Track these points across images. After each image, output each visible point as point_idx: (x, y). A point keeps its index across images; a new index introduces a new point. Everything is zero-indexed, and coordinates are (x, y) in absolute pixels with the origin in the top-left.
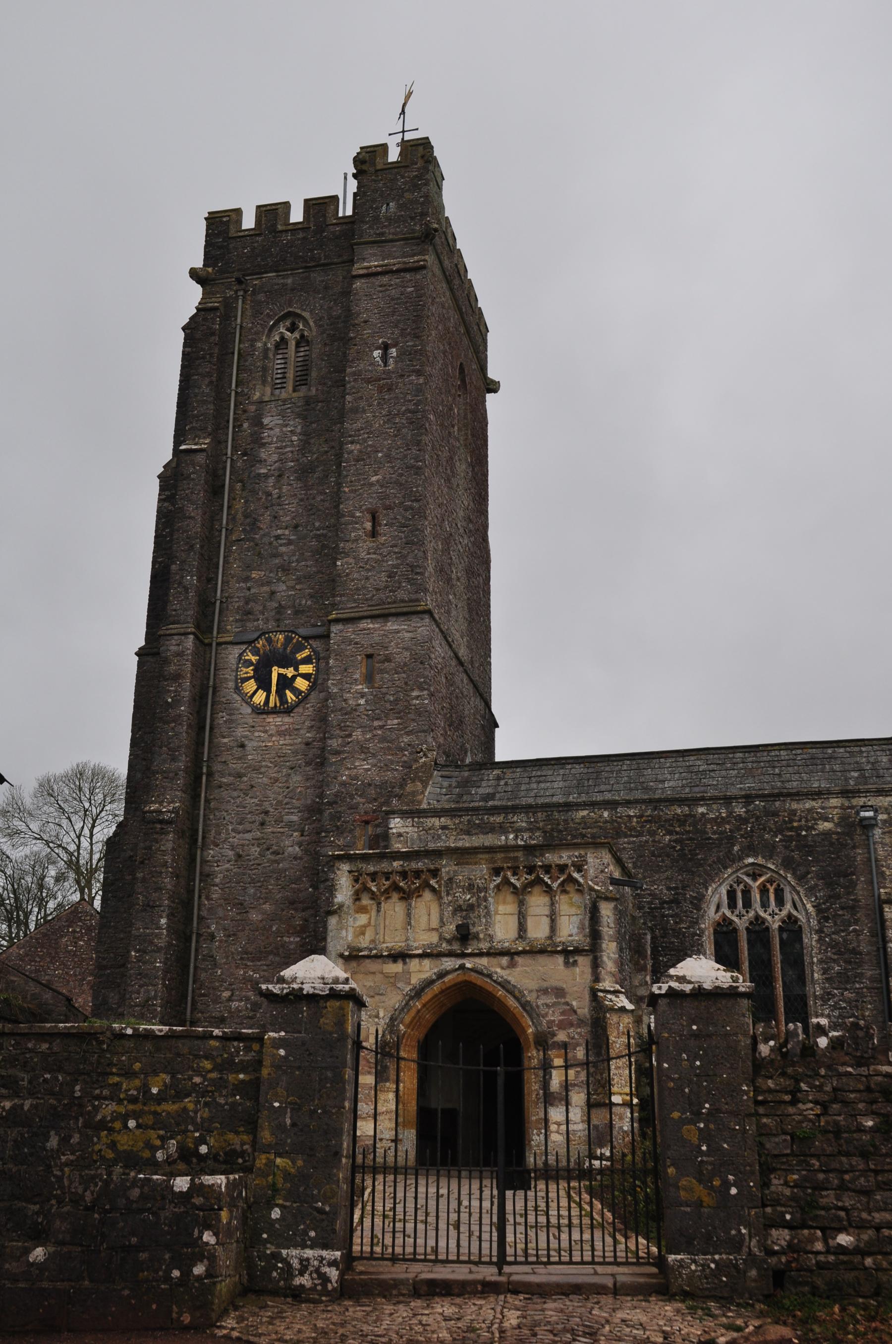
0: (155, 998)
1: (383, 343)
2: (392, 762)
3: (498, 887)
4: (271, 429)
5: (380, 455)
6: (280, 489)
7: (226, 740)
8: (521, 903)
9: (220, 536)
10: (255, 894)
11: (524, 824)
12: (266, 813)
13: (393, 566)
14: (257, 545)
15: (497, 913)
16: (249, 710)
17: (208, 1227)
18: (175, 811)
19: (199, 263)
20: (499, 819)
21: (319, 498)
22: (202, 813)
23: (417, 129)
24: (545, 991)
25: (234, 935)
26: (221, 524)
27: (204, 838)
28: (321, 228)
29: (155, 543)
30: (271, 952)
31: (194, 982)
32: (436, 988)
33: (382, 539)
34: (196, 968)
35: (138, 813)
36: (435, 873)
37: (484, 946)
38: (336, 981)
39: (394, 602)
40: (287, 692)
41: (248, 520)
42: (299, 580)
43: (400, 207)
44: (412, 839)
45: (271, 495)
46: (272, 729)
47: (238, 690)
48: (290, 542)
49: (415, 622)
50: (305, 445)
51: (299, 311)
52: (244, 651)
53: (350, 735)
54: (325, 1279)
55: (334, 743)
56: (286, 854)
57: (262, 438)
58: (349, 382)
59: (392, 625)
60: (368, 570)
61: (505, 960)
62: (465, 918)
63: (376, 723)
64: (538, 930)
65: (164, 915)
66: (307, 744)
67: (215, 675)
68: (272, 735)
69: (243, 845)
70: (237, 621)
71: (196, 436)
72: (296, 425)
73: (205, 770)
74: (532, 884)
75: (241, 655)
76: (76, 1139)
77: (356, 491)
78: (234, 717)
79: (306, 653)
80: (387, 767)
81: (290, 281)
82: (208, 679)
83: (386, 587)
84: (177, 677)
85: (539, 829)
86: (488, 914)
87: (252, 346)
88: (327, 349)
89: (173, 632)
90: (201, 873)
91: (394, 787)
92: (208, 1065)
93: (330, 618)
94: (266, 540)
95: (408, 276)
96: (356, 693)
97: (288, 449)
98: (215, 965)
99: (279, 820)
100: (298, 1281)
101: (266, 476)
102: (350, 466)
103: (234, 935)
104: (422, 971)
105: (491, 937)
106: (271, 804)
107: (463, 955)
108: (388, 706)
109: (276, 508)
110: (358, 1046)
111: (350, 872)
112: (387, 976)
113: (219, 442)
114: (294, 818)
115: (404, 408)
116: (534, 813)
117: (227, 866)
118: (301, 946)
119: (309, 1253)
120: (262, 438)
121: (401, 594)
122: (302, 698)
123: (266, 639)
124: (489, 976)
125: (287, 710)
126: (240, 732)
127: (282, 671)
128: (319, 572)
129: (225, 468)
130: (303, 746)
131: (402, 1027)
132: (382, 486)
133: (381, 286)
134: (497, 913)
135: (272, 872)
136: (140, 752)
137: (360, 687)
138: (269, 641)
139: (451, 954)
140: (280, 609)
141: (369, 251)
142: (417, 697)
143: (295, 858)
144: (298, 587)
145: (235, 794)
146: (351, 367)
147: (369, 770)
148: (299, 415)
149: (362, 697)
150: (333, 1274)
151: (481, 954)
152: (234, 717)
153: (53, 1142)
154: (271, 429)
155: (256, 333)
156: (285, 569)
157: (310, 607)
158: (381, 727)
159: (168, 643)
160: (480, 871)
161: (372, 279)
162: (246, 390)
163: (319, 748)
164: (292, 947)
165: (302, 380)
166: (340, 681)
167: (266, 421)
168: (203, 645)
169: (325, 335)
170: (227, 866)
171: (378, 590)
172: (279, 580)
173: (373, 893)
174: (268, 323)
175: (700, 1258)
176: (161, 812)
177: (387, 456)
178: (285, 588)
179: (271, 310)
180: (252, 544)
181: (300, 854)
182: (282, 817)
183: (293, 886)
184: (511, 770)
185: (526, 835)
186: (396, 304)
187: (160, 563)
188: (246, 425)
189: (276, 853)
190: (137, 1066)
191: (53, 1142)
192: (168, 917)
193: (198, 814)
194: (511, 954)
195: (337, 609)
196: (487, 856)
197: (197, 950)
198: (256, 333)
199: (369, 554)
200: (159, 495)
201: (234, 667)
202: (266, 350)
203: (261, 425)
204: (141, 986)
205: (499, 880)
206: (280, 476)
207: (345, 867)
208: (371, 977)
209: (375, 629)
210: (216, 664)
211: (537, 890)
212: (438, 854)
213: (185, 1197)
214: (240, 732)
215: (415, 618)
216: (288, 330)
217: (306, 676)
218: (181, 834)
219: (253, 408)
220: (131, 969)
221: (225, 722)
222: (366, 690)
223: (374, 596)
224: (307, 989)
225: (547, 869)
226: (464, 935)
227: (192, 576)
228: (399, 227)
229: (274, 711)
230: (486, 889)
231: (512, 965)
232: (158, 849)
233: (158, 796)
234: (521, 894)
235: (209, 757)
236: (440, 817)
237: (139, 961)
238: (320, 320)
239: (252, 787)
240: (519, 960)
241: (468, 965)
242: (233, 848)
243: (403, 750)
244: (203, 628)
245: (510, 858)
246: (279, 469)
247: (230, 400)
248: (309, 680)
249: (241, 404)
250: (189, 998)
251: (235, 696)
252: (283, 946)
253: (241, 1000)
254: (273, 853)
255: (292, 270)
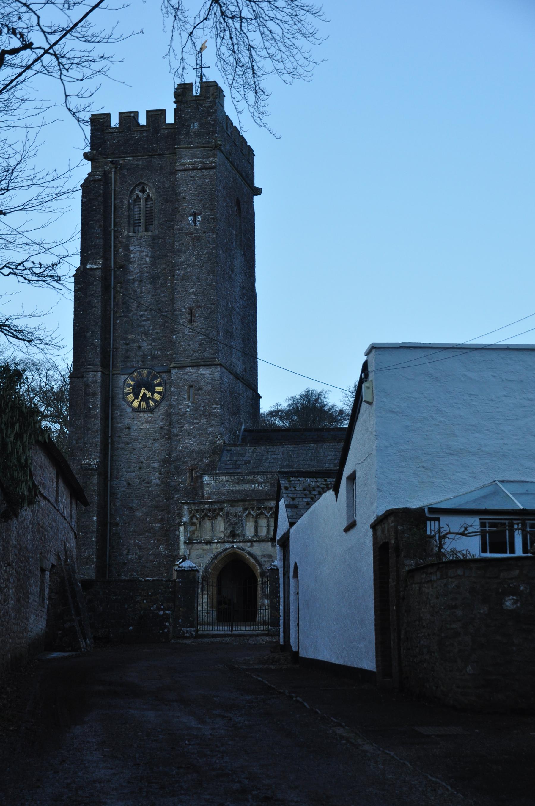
0: (93, 555)
1: (194, 212)
2: (204, 441)
3: (247, 516)
4: (134, 253)
5: (194, 277)
6: (141, 288)
7: (119, 425)
8: (256, 522)
9: (110, 313)
10: (138, 503)
11: (262, 480)
12: (142, 463)
13: (202, 339)
14: (131, 320)
15: (246, 526)
16: (131, 410)
17: (167, 622)
18: (97, 463)
19: (88, 149)
20: (251, 477)
21: (162, 295)
22: (109, 463)
23: (209, 67)
24: (264, 556)
25: (128, 523)
26: (110, 308)
27: (111, 475)
28: (157, 130)
29: (74, 315)
30: (147, 531)
31: (110, 546)
32: (223, 555)
33: (196, 324)
34: (110, 539)
35: (75, 462)
36: (221, 510)
37: (241, 539)
38: (193, 567)
39: (203, 359)
40: (150, 401)
41: (125, 306)
42: (153, 340)
43: (200, 125)
44: (213, 486)
45: (136, 292)
46: (143, 420)
47: (124, 399)
48: (148, 319)
49: (212, 369)
50: (153, 264)
51: (146, 182)
52: (127, 378)
53: (182, 427)
54: (192, 634)
55: (175, 431)
56: (152, 483)
57: (130, 258)
58: (177, 234)
59: (202, 371)
60: (190, 341)
61: (249, 544)
62: (233, 528)
63: (195, 421)
64: (263, 532)
65: (95, 515)
66: (161, 428)
67: (112, 391)
68: (143, 423)
69: (131, 479)
70: (122, 362)
71: (94, 258)
72: (147, 251)
73: (110, 441)
74: (260, 514)
75: (125, 380)
76: (132, 605)
77: (182, 297)
78: (123, 413)
79: (159, 380)
80: (201, 443)
81: (140, 163)
82: (109, 393)
83: (199, 350)
84: (94, 394)
85: (268, 482)
86: (243, 526)
87: (121, 202)
88: (163, 207)
89: (90, 370)
90: (110, 493)
91: (205, 453)
92: (162, 587)
93: (171, 366)
94: (135, 317)
95: (206, 172)
96: (185, 406)
97: (145, 266)
98: (120, 538)
99: (148, 466)
100: (186, 635)
101: (134, 280)
102: (178, 283)
103: (128, 523)
104: (217, 548)
105: (244, 535)
106: (144, 458)
107: (233, 542)
108: (201, 413)
109: (140, 300)
110: (198, 582)
111: (188, 509)
112: (204, 550)
113: (106, 260)
114: (156, 465)
115: (206, 251)
116: (266, 475)
117: (124, 489)
118: (162, 528)
119: (188, 629)
120: (130, 258)
121: (206, 354)
122: (158, 404)
123: (138, 373)
124: (243, 550)
125: (150, 410)
126: (127, 421)
127: (146, 392)
128: (164, 336)
129: (111, 275)
130: (159, 429)
131: (210, 570)
132: (195, 295)
133: (191, 177)
134: (246, 526)
135: (146, 492)
136: (74, 430)
137: (187, 402)
138: (139, 373)
139: (228, 542)
140: (144, 356)
141: (185, 152)
142: (215, 409)
143: (157, 485)
144: (153, 344)
145: (126, 453)
146: (177, 225)
147: (192, 444)
148: (150, 246)
149: (188, 408)
150: (194, 633)
151: (240, 542)
152: (123, 413)
153: (126, 606)
154: (134, 253)
155: (123, 194)
156: (146, 334)
157: (160, 355)
158: (198, 423)
159: (88, 376)
160: (239, 509)
161: (186, 172)
162: (120, 229)
163: (167, 430)
164: (157, 528)
165: (149, 223)
166: (177, 400)
167: (132, 248)
168: (106, 377)
169: (161, 198)
170: (124, 489)
171: (194, 351)
172: (143, 340)
173: (197, 518)
174: (130, 188)
175: (276, 628)
176: (90, 464)
177: (198, 278)
178: (146, 345)
179: (131, 180)
180: (128, 319)
181: (159, 483)
182: (150, 465)
183: (157, 499)
184: (259, 447)
185: (263, 485)
186: (200, 189)
187: (78, 326)
188: (120, 250)
189: (148, 483)
190: (145, 588)
191: (126, 606)
192: (97, 516)
193: (108, 463)
194: (252, 541)
195: (174, 361)
196: (242, 503)
197: (110, 531)
198: (123, 194)
199: (190, 332)
200: (75, 287)
201: (122, 387)
202: (129, 204)
203: (128, 250)
204: (85, 549)
205: (246, 513)
206: (141, 281)
207: (186, 507)
208: (197, 551)
209: (194, 373)
210: (112, 385)
211: (262, 516)
212: (223, 502)
213: (162, 615)
214: (127, 421)
215: (213, 368)
216: (140, 191)
217: (159, 393)
218: (99, 474)
219: (124, 240)
220: (81, 541)
221: (119, 416)
222: (190, 404)
223: (192, 355)
224: (186, 569)
225: (265, 508)
226: (233, 535)
227: (98, 340)
228: (200, 139)
229: (144, 411)
230: (242, 516)
231: (252, 546)
232: (91, 483)
233: (88, 456)
234: (256, 519)
235: (111, 434)
236: (225, 476)
237: (84, 537)
238: (158, 188)
239: (134, 449)
240: (255, 544)
241: (235, 546)
242: (126, 480)
243: (209, 434)
244: (105, 365)
245: (251, 504)
246: (140, 277)
247: (111, 235)
248: (160, 395)
249: (117, 237)
250: (108, 554)
251: (123, 402)
252: (152, 528)
253: (133, 554)
254: (146, 483)
255: (141, 156)
